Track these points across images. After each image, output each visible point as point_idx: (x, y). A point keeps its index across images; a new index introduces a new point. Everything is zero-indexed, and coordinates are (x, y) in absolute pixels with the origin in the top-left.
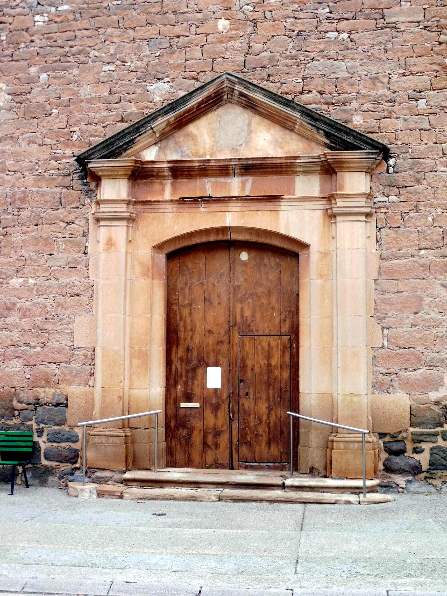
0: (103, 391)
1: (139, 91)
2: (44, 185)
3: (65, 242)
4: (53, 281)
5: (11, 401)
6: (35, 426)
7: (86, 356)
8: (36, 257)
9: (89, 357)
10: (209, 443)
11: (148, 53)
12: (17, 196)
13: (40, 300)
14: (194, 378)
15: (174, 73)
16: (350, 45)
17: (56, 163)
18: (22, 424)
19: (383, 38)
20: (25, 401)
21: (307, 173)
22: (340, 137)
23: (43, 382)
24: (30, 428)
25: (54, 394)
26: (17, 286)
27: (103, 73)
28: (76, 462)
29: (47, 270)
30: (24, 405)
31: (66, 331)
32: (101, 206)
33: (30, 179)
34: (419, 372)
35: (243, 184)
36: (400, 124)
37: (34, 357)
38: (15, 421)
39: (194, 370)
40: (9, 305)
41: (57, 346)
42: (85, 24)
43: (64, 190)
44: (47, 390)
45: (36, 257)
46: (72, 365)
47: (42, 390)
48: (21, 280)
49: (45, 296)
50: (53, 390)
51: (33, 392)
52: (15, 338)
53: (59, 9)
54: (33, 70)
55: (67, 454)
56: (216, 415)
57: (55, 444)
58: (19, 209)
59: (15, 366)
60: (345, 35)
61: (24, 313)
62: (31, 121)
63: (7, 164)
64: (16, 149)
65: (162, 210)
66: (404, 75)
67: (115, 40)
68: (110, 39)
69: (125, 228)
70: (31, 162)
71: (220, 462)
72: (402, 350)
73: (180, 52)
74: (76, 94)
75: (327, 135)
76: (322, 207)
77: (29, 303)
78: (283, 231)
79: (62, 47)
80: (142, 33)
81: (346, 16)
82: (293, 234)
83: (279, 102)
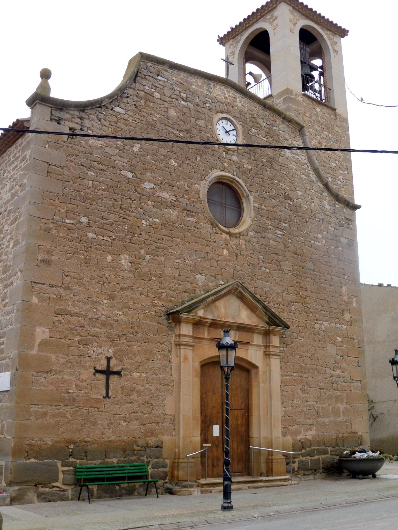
0: (184, 438)
1: (192, 277)
2: (149, 320)
3: (160, 354)
4: (154, 376)
5: (133, 445)
6: (146, 460)
7: (171, 419)
8: (145, 361)
9: (173, 419)
10: (215, 465)
11: (195, 258)
12: (135, 324)
13: (148, 386)
14: (208, 431)
15: (207, 272)
16: (269, 275)
17: (154, 309)
18: (139, 459)
19: (280, 275)
20: (141, 445)
21: (258, 333)
22: (274, 321)
23: (150, 434)
24: (143, 461)
25: (155, 440)
26: (136, 377)
27: (175, 263)
28: (166, 479)
29: (151, 369)
30: (140, 447)
31: (162, 405)
32: (181, 337)
33: (141, 315)
34: (294, 427)
35: (235, 334)
36: (286, 315)
37: (145, 419)
38: (134, 458)
39: (208, 426)
40: (132, 388)
41: (157, 413)
42: (167, 233)
43: (159, 325)
44: (152, 438)
45: (145, 361)
46: (164, 424)
47: (150, 438)
48: (138, 374)
49: (150, 384)
50: (155, 439)
51: (145, 440)
52: (135, 408)
53: (154, 220)
54: (142, 251)
55: (162, 475)
56: (217, 450)
57: (156, 470)
58: (137, 332)
59: (135, 425)
60: (268, 270)
61: (140, 394)
62: (141, 281)
63: (129, 304)
64: (134, 296)
65: (203, 343)
66: (287, 294)
67: (181, 246)
68: (179, 245)
69: (192, 351)
70: (142, 305)
71: (220, 474)
72: (288, 418)
73: (209, 261)
74: (163, 271)
75: (269, 318)
76: (262, 350)
77: (142, 388)
78: (249, 360)
79: (156, 243)
80: (192, 246)
81: (268, 261)
82: (254, 362)
83: (255, 300)
